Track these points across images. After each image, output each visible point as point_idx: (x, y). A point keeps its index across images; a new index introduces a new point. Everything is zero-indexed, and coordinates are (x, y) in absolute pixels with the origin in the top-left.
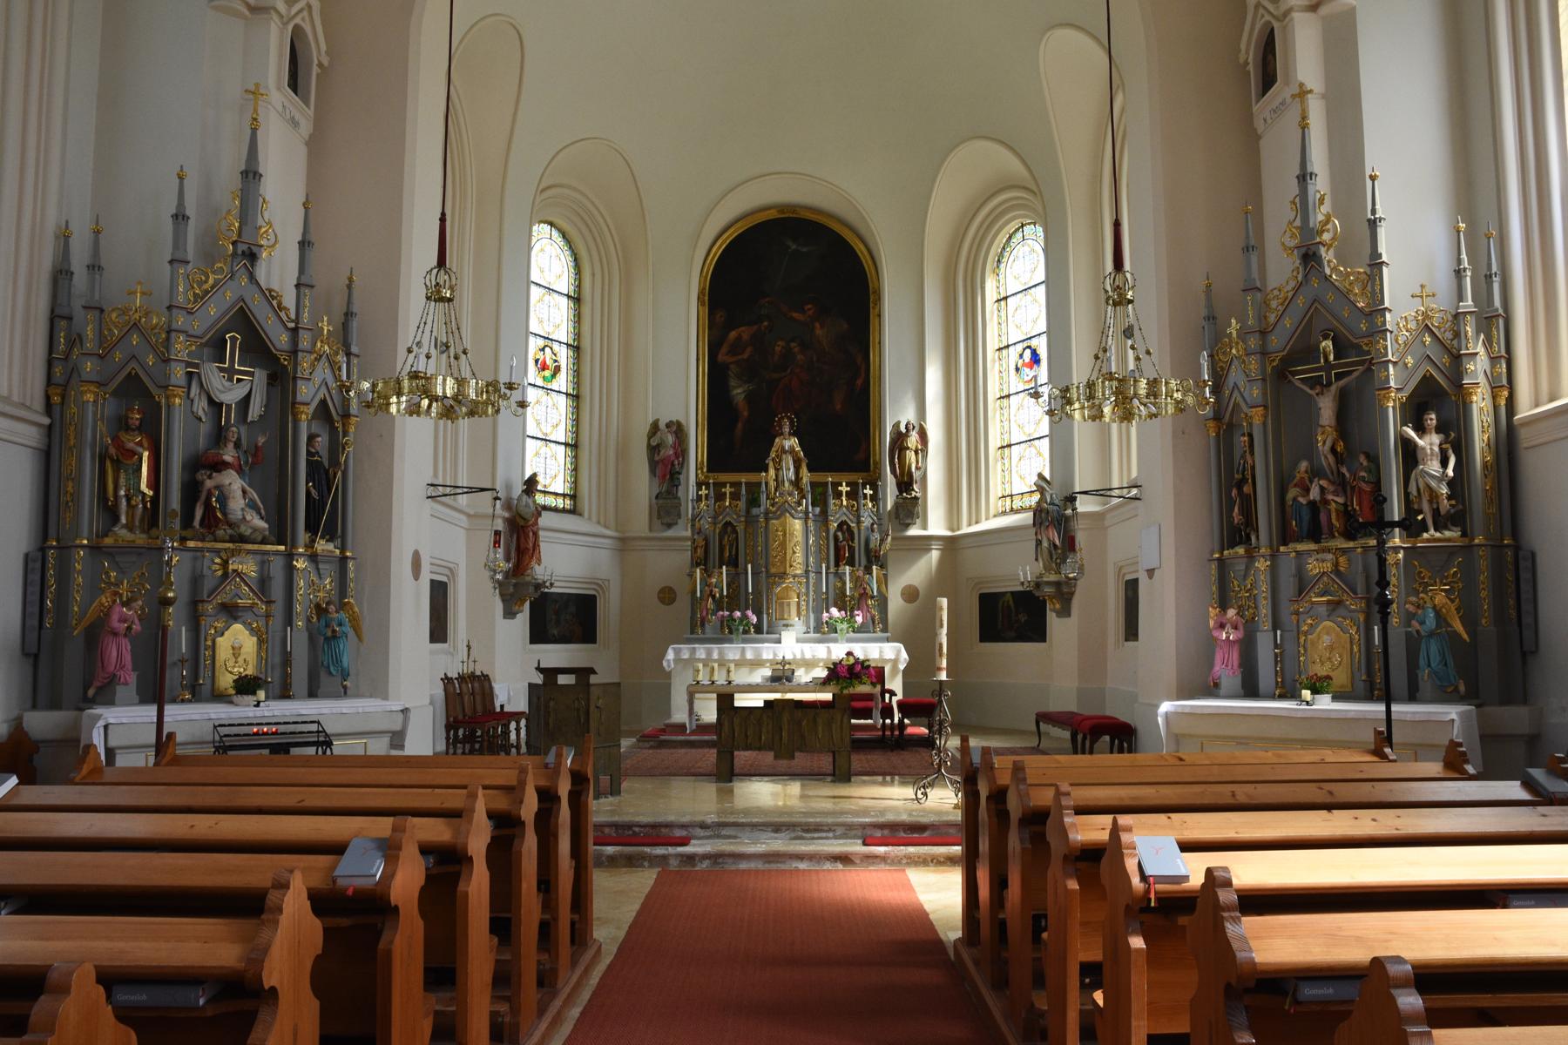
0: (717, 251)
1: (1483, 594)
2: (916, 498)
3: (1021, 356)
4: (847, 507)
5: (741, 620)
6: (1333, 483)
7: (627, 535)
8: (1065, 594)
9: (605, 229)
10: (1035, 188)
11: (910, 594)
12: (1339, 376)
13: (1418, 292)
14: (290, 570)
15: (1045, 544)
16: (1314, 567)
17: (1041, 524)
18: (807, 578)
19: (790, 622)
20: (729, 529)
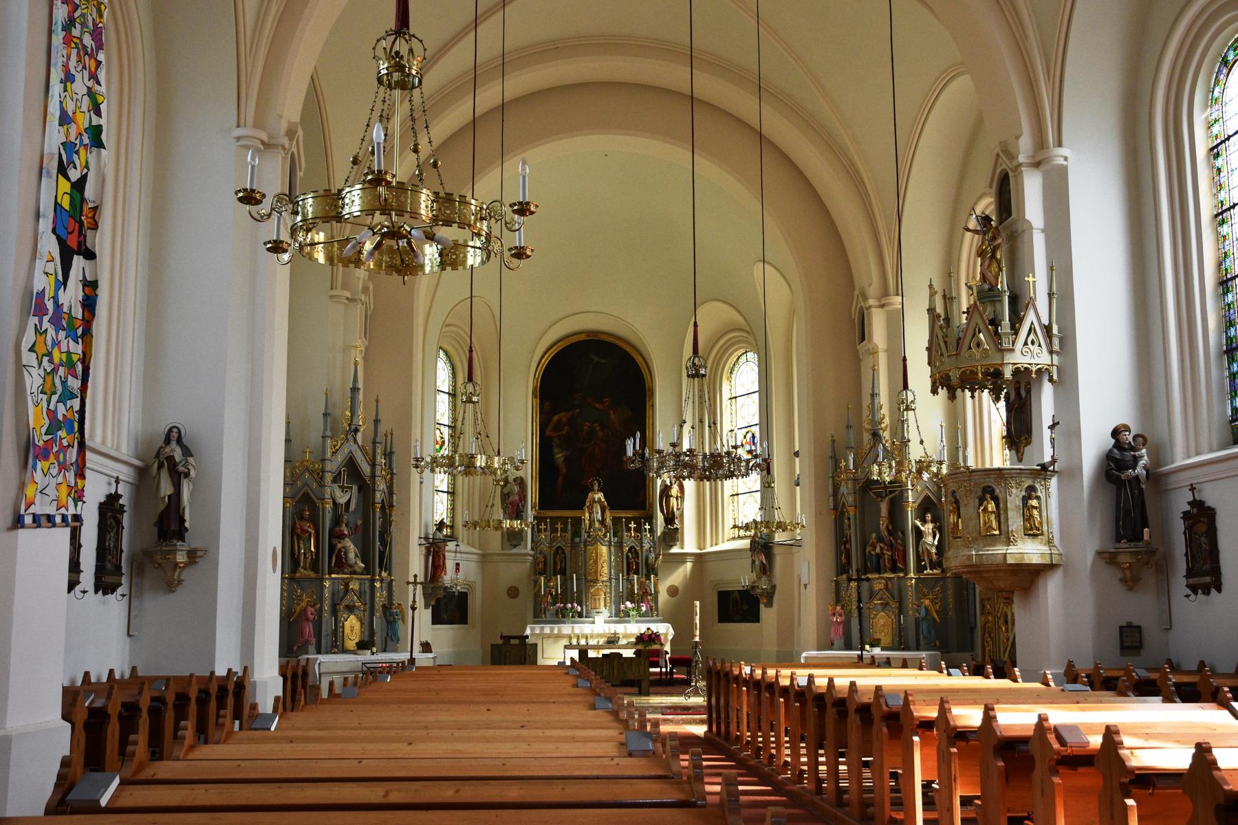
0: (545, 361)
1: (950, 600)
2: (677, 529)
3: (745, 437)
4: (634, 537)
6: (886, 545)
8: (770, 595)
10: (748, 329)
11: (673, 591)
12: (891, 492)
14: (373, 587)
15: (757, 563)
16: (879, 586)
17: (755, 550)
18: (611, 583)
19: (601, 610)
20: (560, 551)
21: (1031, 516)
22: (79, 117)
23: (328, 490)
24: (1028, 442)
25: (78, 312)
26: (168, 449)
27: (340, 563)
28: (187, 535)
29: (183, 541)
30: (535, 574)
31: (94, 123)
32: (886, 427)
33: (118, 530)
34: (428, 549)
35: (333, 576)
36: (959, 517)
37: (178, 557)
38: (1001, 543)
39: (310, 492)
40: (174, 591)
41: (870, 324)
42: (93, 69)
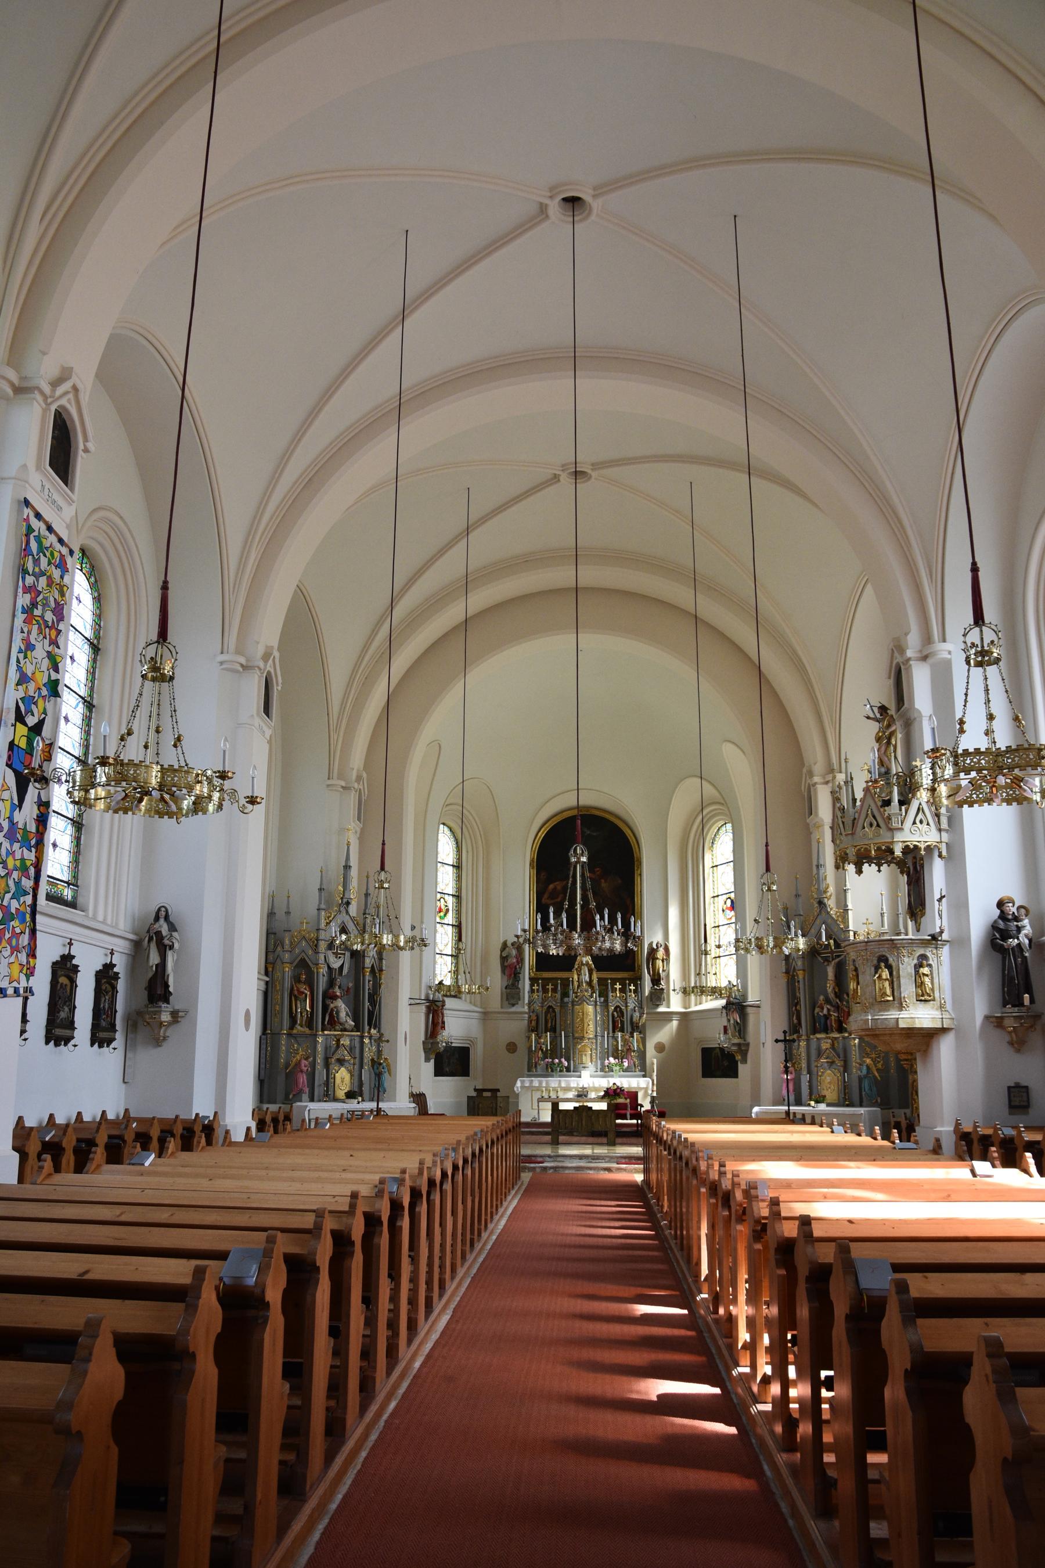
0: (542, 835)
2: (662, 989)
5: (559, 1064)
7: (490, 1010)
8: (744, 1054)
9: (476, 827)
10: (723, 802)
11: (660, 1048)
12: (839, 956)
13: (865, 921)
14: (362, 1043)
18: (596, 1040)
21: (922, 983)
22: (38, 675)
23: (322, 957)
24: (923, 914)
25: (32, 827)
26: (156, 926)
27: (332, 1021)
28: (171, 998)
29: (168, 1003)
30: (529, 1031)
31: (52, 678)
32: (831, 896)
33: (113, 994)
34: (428, 1008)
35: (326, 1032)
36: (858, 983)
37: (162, 1017)
38: (893, 1008)
39: (307, 959)
40: (160, 1046)
41: (816, 802)
42: (53, 637)
